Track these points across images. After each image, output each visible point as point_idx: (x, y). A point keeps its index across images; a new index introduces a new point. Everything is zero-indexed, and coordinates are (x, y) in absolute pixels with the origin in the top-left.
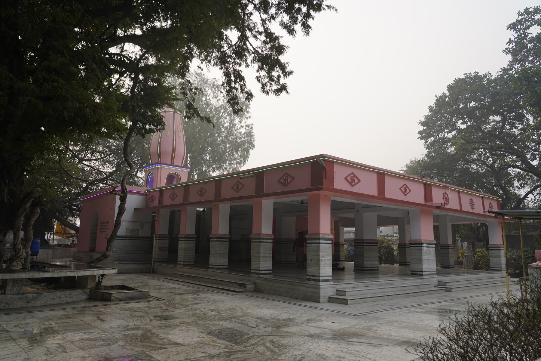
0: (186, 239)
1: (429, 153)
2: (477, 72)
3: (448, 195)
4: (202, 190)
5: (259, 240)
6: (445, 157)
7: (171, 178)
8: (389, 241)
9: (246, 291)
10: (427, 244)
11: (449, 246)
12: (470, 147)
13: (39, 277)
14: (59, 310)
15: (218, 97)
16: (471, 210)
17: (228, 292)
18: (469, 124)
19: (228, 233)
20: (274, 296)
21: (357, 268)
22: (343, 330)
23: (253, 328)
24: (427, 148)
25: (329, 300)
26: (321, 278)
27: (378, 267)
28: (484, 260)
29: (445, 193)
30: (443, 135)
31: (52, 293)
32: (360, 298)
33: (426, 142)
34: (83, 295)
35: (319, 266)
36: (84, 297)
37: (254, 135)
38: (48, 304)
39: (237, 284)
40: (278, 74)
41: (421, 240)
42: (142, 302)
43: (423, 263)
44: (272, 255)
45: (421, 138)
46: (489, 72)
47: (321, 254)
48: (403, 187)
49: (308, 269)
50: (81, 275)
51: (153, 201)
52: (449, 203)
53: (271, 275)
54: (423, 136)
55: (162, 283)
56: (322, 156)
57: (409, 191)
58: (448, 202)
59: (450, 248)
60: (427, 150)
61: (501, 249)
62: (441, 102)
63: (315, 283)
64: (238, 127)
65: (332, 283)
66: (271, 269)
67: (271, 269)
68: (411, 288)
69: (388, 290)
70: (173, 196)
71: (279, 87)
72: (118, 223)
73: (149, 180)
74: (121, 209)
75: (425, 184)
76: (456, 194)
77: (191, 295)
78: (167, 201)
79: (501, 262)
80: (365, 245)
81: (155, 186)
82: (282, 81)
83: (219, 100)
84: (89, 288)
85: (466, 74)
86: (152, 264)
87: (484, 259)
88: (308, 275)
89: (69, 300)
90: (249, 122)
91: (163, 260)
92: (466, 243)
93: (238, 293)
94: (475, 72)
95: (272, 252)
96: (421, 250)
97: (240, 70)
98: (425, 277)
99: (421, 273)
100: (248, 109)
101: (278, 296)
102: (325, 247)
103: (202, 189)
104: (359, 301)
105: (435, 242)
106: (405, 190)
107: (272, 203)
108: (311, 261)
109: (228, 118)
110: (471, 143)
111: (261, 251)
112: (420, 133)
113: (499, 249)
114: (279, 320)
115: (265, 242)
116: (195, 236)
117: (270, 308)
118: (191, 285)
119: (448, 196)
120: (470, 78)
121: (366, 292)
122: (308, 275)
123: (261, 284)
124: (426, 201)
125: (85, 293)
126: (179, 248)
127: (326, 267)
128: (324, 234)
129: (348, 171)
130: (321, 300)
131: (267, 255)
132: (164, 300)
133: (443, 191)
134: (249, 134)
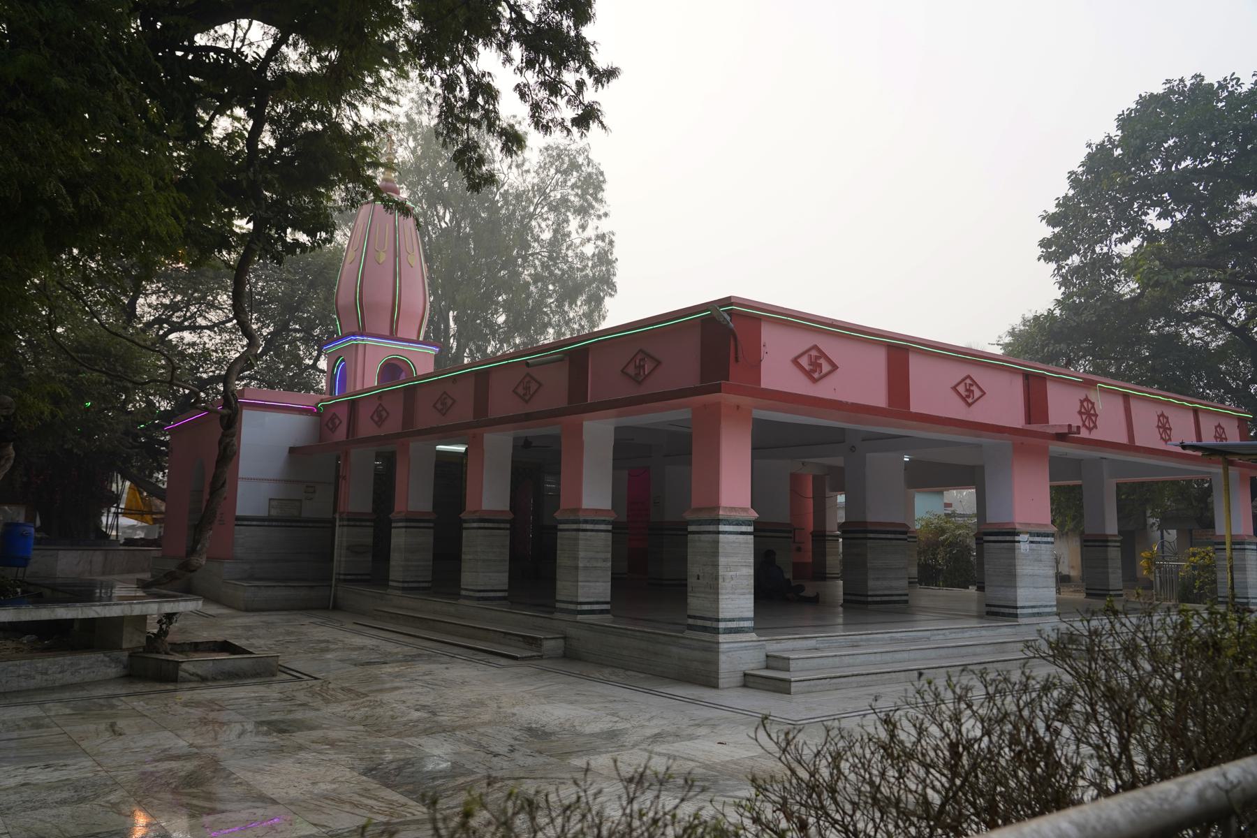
0: (408, 524)
1: (1067, 296)
2: (1200, 76)
3: (1093, 404)
4: (445, 399)
5: (575, 526)
6: (1109, 307)
7: (392, 369)
8: (958, 527)
9: (541, 657)
10: (1032, 534)
11: (1108, 541)
12: (1176, 277)
13: (53, 617)
14: (27, 704)
15: (523, 164)
16: (1161, 446)
17: (492, 659)
18: (1179, 216)
19: (508, 509)
20: (607, 671)
21: (849, 597)
22: (735, 764)
23: (496, 755)
24: (1061, 285)
25: (745, 680)
26: (722, 625)
27: (907, 595)
28: (1207, 577)
29: (1087, 400)
30: (1105, 249)
31: (23, 662)
32: (825, 676)
33: (1059, 268)
34: (110, 667)
35: (718, 594)
36: (113, 671)
37: (617, 259)
38: (14, 689)
39: (521, 639)
40: (578, 76)
41: (1013, 523)
42: (254, 684)
43: (1019, 584)
44: (609, 564)
45: (1047, 258)
46: (1234, 73)
47: (722, 560)
48: (963, 384)
49: (690, 600)
50: (96, 616)
51: (334, 429)
52: (1095, 427)
53: (609, 616)
54: (1054, 250)
55: (339, 635)
56: (728, 301)
57: (958, 388)
58: (1094, 423)
59: (1109, 544)
60: (1063, 289)
61: (1248, 547)
62: (1099, 159)
63: (706, 636)
64: (578, 241)
65: (753, 636)
66: (609, 599)
67: (609, 599)
68: (978, 650)
69: (912, 655)
70: (380, 417)
71: (580, 112)
72: (221, 482)
73: (339, 378)
74: (225, 449)
75: (1027, 376)
76: (1119, 402)
77: (392, 667)
78: (367, 427)
79: (1246, 582)
80: (870, 538)
81: (349, 389)
82: (589, 95)
83: (528, 171)
84: (128, 649)
85: (1168, 81)
86: (331, 586)
87: (1207, 575)
88: (690, 617)
89: (68, 678)
90: (605, 226)
91: (359, 577)
92: (1175, 531)
93: (519, 662)
94: (1196, 76)
95: (609, 555)
96: (1013, 549)
97: (489, 73)
98: (1021, 621)
99: (1011, 611)
100: (599, 196)
101: (616, 670)
102: (734, 542)
103: (445, 396)
104: (822, 685)
105: (753, 515)
106: (967, 390)
107: (612, 428)
108: (698, 579)
109: (552, 216)
110: (1177, 267)
111: (582, 554)
112: (1044, 243)
113: (1242, 547)
114: (580, 735)
115: (592, 530)
116: (510, 516)
117: (576, 701)
118: (411, 640)
119: (1093, 407)
120: (1182, 93)
121: (847, 660)
122: (690, 617)
123: (579, 639)
124: (1029, 420)
125: (117, 661)
126: (392, 546)
127: (736, 596)
128: (732, 509)
129: (802, 342)
130: (721, 681)
131: (595, 565)
132: (316, 679)
133: (1081, 394)
134: (604, 258)
